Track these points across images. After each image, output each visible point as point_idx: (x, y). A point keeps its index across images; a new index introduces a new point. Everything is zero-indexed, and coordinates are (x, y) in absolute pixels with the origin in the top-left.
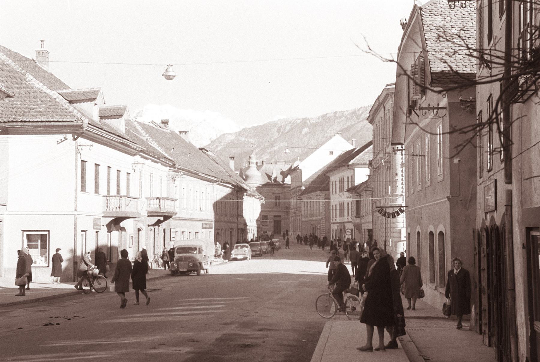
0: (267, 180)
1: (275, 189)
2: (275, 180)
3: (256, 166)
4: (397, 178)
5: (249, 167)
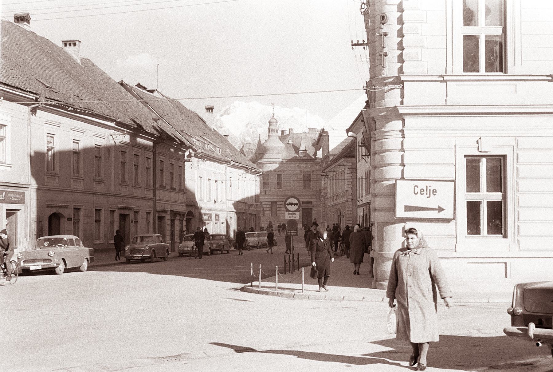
0: (293, 154)
1: (303, 165)
4: (385, 28)
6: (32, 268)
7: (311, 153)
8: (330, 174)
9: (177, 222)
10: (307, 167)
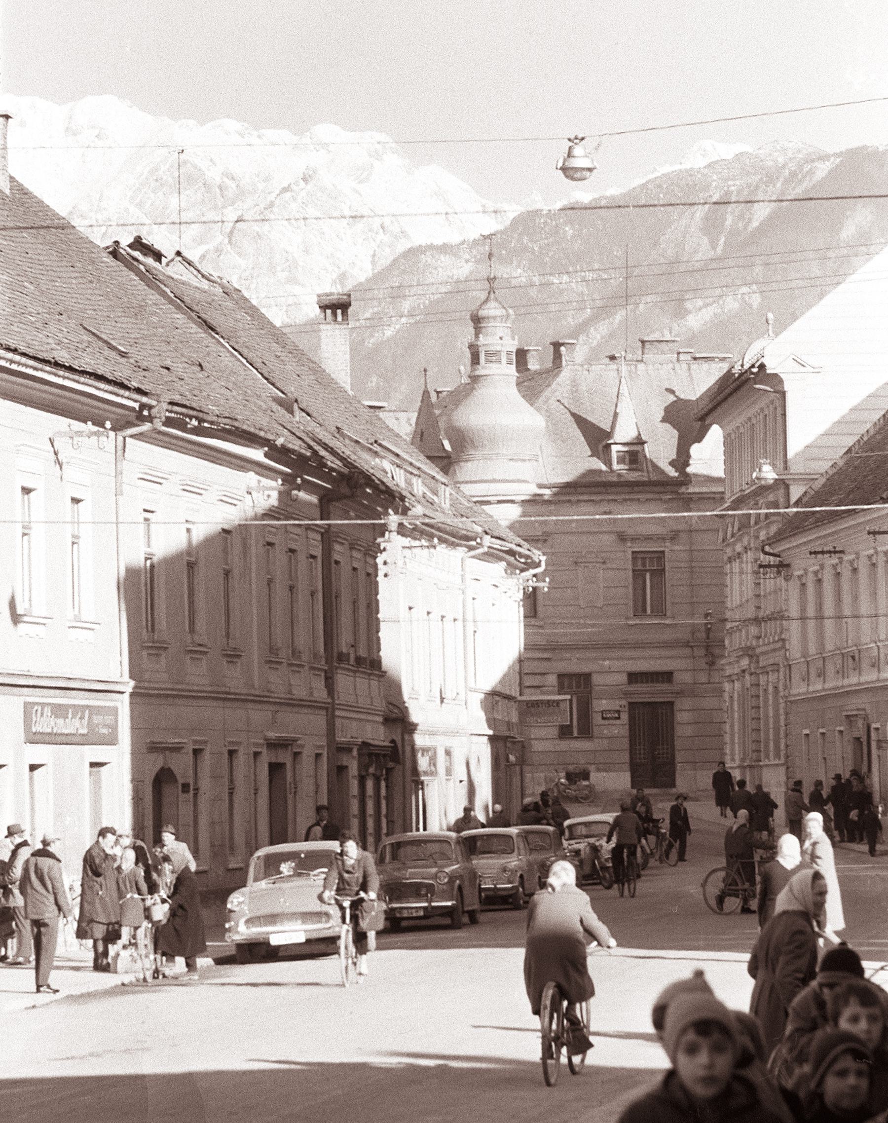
0: (582, 461)
2: (635, 454)
3: (512, 369)
5: (475, 379)
6: (275, 941)
7: (661, 450)
8: (803, 564)
9: (370, 784)
10: (646, 516)
